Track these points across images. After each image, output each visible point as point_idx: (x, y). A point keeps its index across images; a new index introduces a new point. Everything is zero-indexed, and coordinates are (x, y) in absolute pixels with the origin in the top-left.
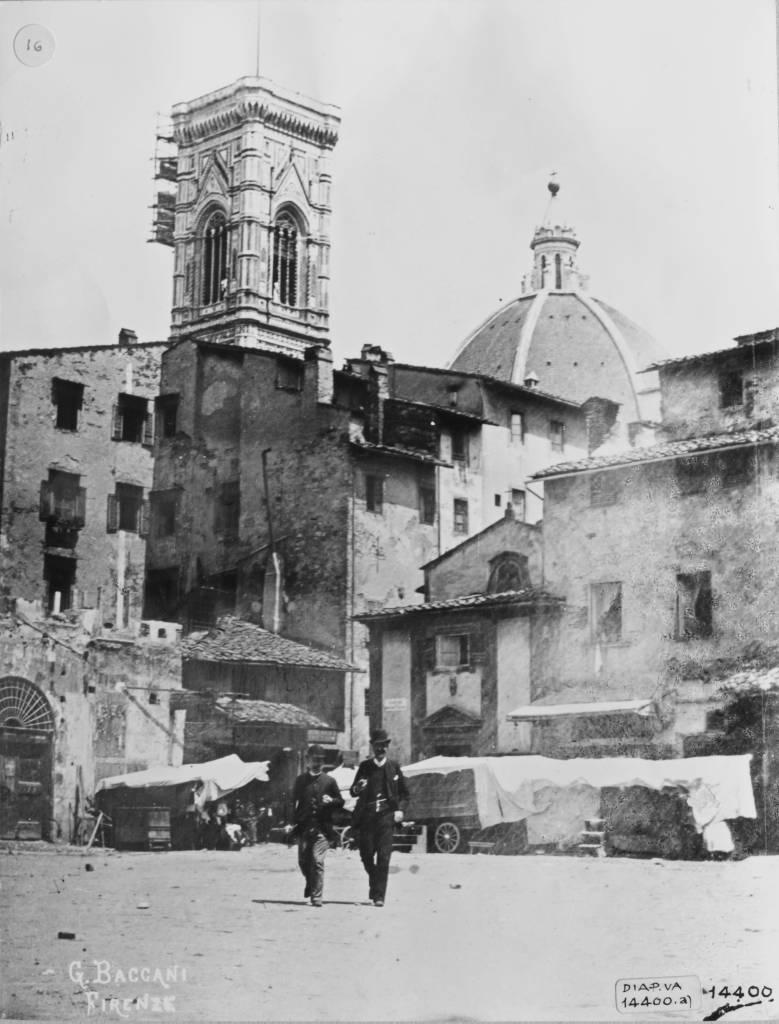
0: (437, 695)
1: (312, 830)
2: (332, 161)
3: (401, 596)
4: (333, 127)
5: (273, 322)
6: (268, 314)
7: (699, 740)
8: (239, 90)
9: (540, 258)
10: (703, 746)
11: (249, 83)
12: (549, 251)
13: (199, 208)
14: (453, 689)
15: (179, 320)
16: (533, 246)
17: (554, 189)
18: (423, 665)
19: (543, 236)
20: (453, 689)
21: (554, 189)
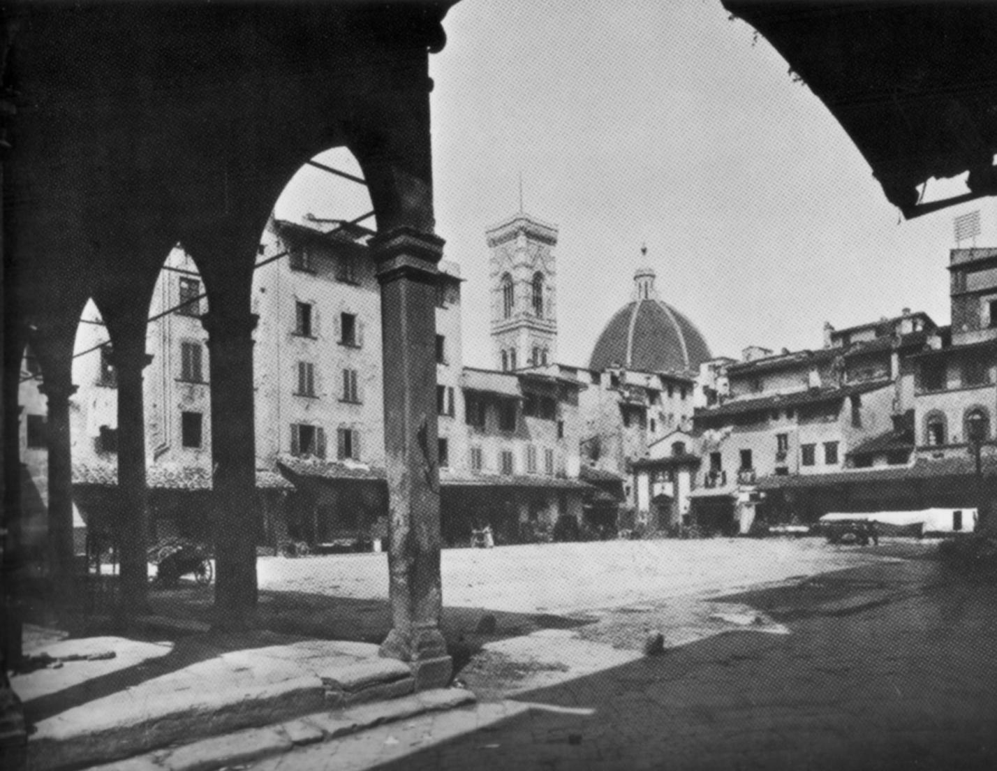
0: (658, 490)
1: (602, 529)
2: (554, 251)
3: (304, 311)
4: (552, 234)
5: (535, 326)
6: (533, 323)
7: (742, 597)
8: (515, 220)
9: (638, 284)
10: (431, 477)
11: (519, 216)
12: (642, 281)
13: (500, 274)
14: (663, 488)
15: (494, 326)
16: (635, 278)
17: (644, 251)
18: (652, 481)
19: (639, 273)
20: (663, 488)
21: (644, 251)
